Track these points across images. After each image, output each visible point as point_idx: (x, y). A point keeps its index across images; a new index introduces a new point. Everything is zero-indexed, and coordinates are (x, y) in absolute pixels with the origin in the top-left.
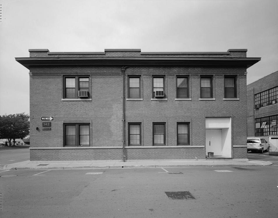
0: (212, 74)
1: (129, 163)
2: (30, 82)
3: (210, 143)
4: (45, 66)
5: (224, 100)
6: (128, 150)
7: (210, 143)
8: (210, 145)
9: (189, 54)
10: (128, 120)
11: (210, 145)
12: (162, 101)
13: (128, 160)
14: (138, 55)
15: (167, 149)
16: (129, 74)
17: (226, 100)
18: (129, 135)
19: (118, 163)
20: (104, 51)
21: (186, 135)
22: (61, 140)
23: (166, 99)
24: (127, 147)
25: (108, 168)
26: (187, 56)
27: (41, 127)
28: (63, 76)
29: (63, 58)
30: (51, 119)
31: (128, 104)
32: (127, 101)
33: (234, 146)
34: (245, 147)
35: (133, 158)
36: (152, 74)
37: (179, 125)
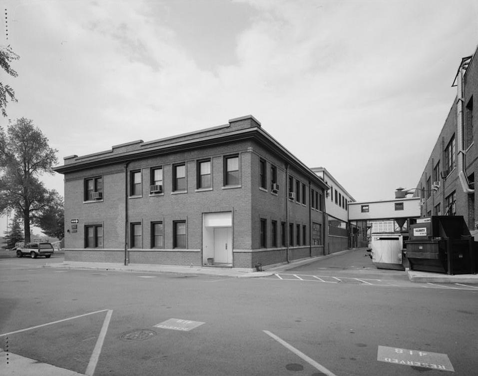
0: (210, 157)
1: (132, 267)
2: (65, 187)
3: (226, 247)
4: (195, 148)
5: (223, 189)
6: (130, 253)
7: (226, 247)
8: (226, 249)
9: (185, 136)
10: (131, 220)
11: (226, 249)
12: (159, 196)
13: (129, 264)
14: (138, 147)
15: (163, 253)
16: (131, 170)
17: (225, 189)
18: (426, 244)
19: (119, 267)
20: (111, 149)
21: (177, 235)
22: (82, 242)
23: (163, 194)
24: (129, 250)
25: (97, 270)
26: (96, 157)
27: (71, 230)
28: (197, 161)
29: (102, 158)
30: (77, 221)
31: (130, 201)
32: (130, 199)
33: (235, 251)
34: (248, 252)
35: (135, 262)
36: (149, 167)
37: (181, 224)
